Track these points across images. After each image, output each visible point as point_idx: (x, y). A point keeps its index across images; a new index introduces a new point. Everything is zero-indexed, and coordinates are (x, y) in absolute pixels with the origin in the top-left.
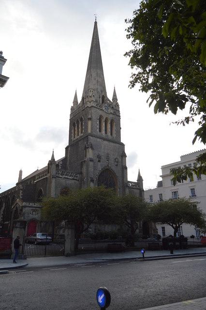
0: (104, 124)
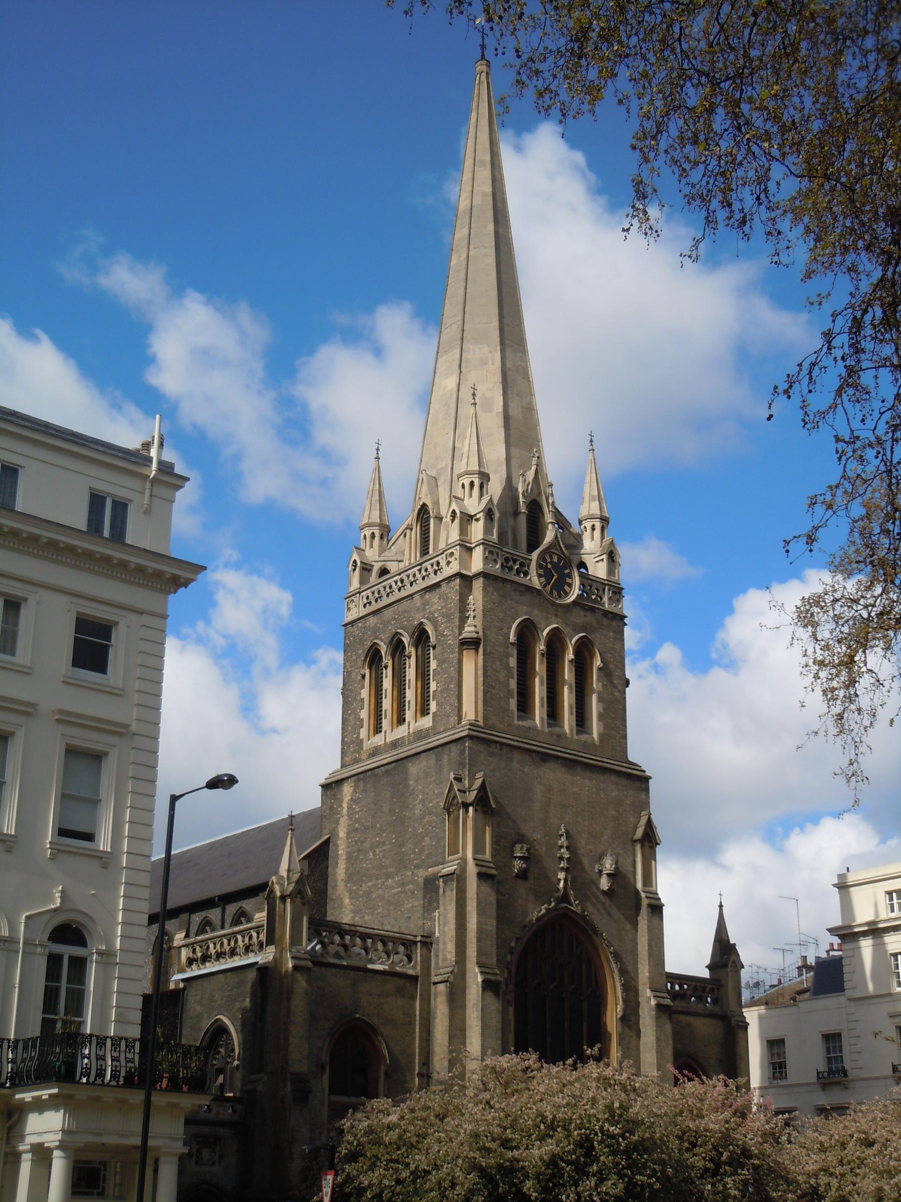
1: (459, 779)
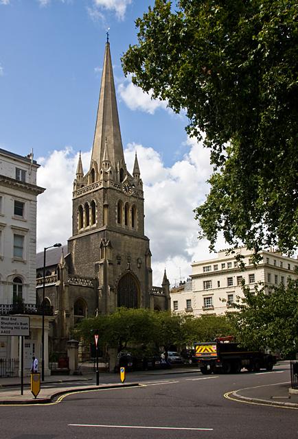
0: (123, 213)
1: (104, 240)
